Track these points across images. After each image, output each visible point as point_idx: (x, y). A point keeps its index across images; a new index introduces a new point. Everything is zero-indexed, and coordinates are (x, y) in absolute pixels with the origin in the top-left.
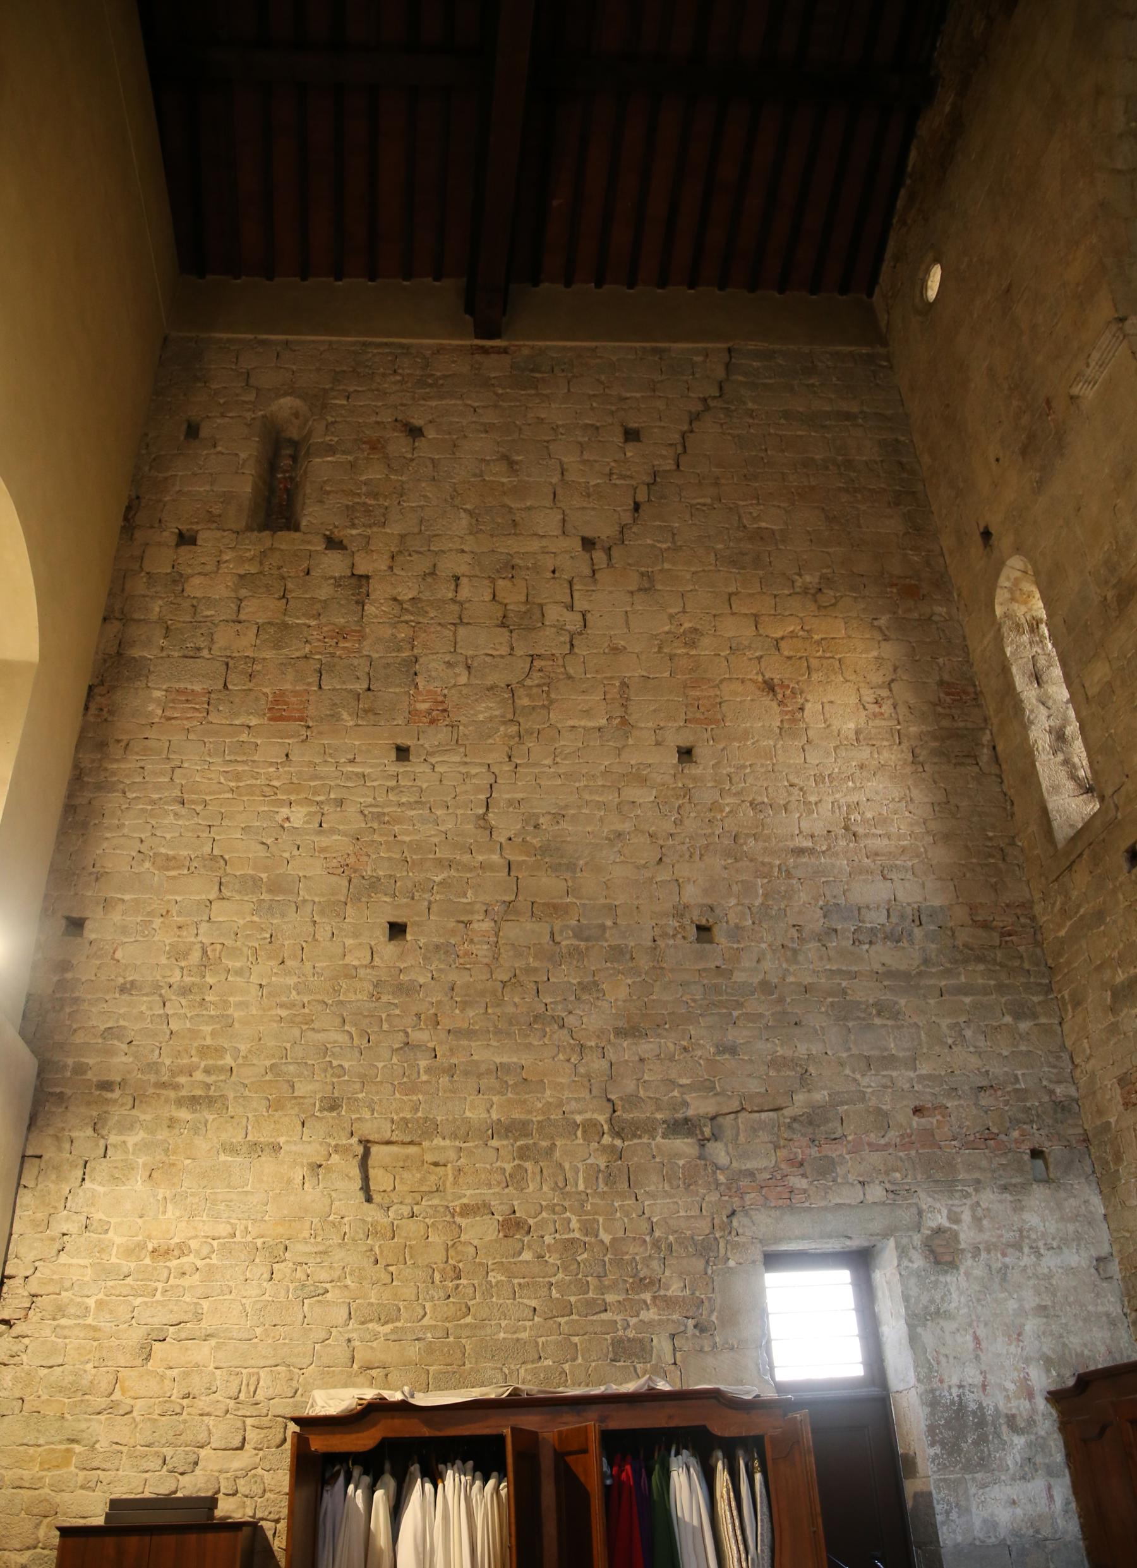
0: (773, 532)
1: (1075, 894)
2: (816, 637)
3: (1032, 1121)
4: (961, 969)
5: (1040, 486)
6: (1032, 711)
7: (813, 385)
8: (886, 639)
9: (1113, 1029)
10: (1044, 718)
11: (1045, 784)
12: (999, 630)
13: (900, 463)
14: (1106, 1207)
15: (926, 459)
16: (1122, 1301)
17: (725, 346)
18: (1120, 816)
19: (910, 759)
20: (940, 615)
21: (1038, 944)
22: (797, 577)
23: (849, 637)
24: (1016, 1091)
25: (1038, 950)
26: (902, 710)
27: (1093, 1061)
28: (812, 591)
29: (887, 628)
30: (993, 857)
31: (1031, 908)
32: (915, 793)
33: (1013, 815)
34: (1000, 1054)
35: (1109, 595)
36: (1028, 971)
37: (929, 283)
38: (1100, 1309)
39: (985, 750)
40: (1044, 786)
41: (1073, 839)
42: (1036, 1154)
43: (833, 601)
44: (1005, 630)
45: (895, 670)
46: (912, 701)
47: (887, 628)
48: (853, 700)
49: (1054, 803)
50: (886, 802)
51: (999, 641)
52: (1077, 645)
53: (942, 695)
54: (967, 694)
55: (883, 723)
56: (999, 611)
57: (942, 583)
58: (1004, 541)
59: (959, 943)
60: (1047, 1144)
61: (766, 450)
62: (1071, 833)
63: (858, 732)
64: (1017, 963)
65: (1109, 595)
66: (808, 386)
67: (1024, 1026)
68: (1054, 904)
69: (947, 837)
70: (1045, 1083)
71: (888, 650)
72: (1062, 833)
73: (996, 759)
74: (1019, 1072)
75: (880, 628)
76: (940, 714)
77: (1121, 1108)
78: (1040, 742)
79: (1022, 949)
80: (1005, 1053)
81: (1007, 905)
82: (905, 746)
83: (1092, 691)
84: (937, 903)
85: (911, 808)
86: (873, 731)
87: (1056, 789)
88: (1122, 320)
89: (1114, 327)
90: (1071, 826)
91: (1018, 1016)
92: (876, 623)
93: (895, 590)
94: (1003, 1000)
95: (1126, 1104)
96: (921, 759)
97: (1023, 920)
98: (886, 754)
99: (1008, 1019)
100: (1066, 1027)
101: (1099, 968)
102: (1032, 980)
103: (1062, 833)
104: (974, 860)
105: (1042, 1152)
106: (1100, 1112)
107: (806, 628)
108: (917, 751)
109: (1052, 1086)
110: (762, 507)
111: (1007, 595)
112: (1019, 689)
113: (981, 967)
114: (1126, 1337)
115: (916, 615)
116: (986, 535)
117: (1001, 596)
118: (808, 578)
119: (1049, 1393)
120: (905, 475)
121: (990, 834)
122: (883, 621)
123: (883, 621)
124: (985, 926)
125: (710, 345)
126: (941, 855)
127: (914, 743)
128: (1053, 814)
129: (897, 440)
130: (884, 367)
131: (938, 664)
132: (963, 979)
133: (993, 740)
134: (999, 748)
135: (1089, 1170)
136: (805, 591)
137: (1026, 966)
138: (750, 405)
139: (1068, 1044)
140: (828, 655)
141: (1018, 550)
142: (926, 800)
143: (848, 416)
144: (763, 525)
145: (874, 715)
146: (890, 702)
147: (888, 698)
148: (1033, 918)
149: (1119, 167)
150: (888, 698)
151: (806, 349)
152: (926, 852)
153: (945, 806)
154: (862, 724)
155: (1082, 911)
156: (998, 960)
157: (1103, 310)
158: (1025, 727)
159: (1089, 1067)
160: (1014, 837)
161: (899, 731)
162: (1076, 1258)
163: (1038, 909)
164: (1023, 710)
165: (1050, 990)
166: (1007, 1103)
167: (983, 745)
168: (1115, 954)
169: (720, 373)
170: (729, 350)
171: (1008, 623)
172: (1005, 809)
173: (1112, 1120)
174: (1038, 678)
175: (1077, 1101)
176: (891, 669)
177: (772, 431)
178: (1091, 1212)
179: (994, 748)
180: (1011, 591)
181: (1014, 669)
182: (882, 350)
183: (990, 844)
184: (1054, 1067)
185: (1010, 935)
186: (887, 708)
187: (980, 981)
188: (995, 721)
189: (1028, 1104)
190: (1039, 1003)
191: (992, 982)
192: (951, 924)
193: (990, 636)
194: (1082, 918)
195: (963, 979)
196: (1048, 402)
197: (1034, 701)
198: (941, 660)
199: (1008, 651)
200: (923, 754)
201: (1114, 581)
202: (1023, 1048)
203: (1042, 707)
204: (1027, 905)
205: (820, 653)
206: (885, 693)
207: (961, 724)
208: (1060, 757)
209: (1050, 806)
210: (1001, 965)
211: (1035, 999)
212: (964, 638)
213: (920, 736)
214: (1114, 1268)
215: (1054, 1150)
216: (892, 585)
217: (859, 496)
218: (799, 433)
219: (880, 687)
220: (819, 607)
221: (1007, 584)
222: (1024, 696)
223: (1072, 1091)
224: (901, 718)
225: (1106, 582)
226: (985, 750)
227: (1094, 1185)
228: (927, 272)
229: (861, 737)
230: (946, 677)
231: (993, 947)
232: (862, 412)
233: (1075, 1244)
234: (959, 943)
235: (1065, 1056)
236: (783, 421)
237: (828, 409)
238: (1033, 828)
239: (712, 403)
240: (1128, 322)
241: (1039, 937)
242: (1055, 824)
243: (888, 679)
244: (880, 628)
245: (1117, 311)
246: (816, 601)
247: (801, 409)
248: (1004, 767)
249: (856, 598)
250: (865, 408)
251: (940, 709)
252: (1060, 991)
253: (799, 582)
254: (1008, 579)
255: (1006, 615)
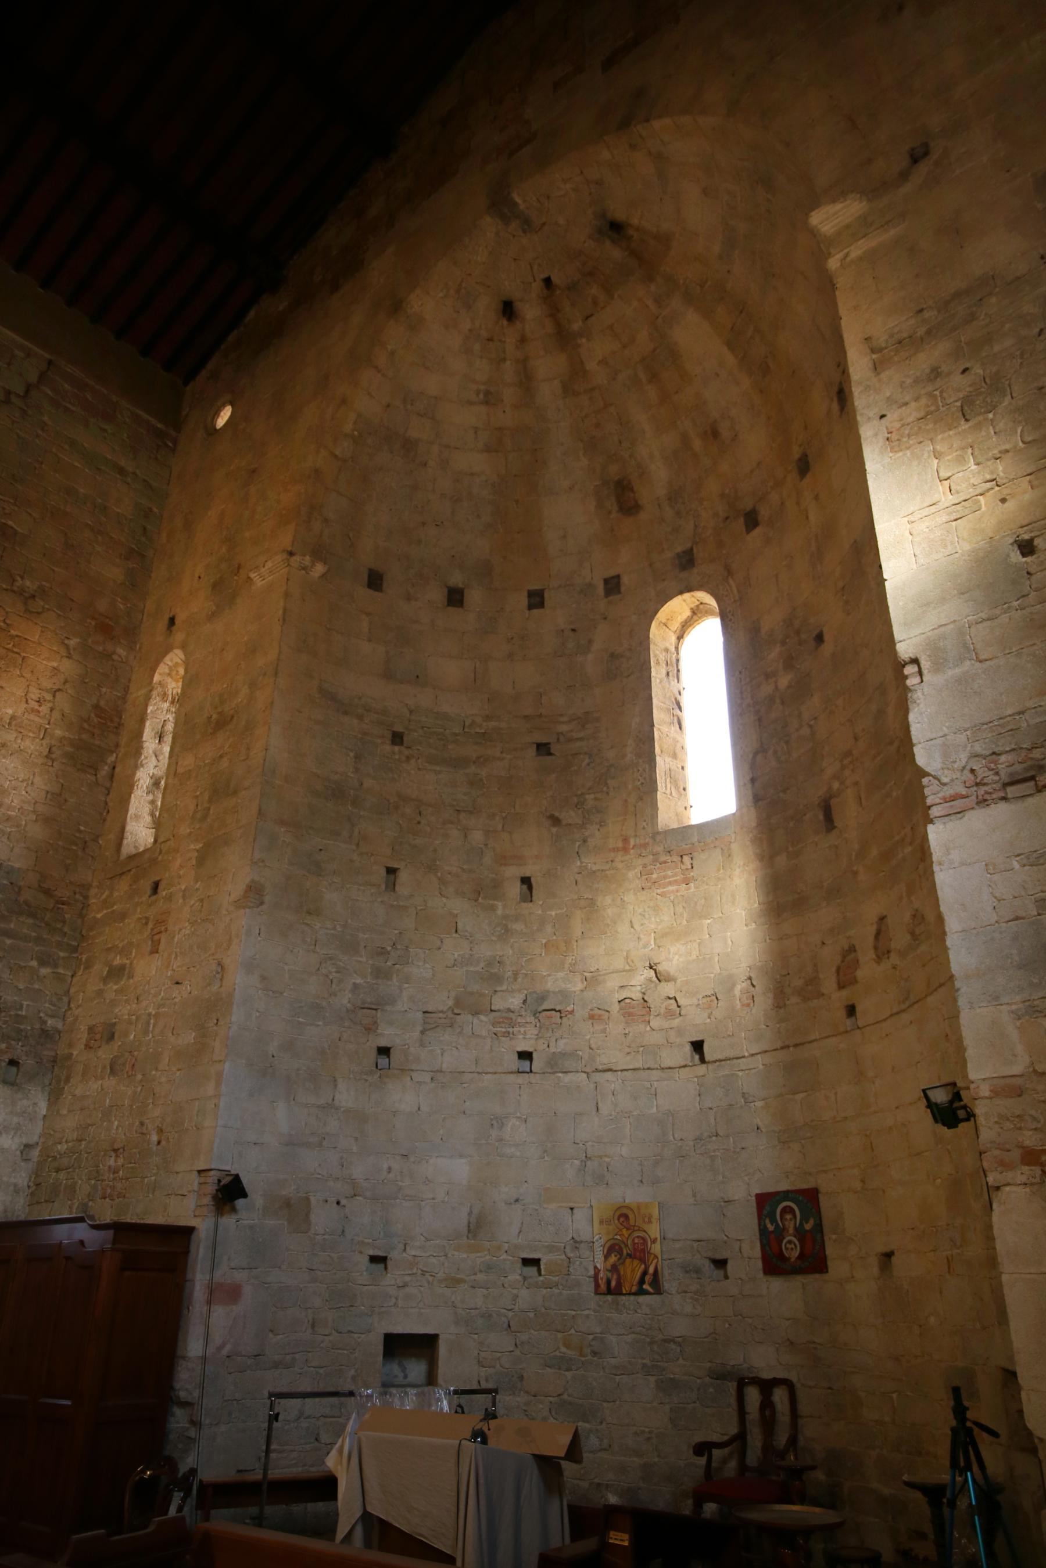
0: (16, 532)
1: (116, 894)
2: (13, 632)
3: (19, 1040)
4: (14, 919)
5: (212, 617)
6: (146, 758)
7: (105, 430)
8: (69, 657)
9: (100, 993)
10: (152, 766)
11: (132, 811)
12: (151, 691)
13: (145, 529)
14: (48, 1110)
15: (164, 535)
16: (30, 1177)
17: (47, 356)
18: (160, 858)
19: (45, 753)
20: (120, 656)
21: (81, 916)
22: (19, 578)
23: (40, 644)
24: (18, 1015)
25: (79, 921)
26: (56, 715)
27: (80, 1010)
28: (27, 595)
29: (74, 649)
30: (77, 845)
31: (88, 889)
32: (38, 780)
33: (104, 820)
34: (16, 987)
35: (215, 716)
36: (65, 933)
37: (222, 414)
38: (13, 1180)
39: (106, 768)
40: (130, 813)
41: (131, 858)
42: (13, 1063)
43: (40, 610)
44: (154, 693)
45: (64, 683)
46: (67, 711)
47: (74, 649)
48: (20, 693)
49: (131, 826)
50: (10, 778)
51: (148, 698)
52: (187, 735)
53: (93, 715)
54: (112, 721)
55: (37, 719)
56: (157, 678)
57: (131, 633)
58: (179, 636)
59: (21, 899)
60: (24, 1058)
61: (42, 463)
62: (134, 851)
63: (13, 718)
64: (59, 926)
65: (215, 716)
66: (101, 429)
67: (44, 971)
68: (102, 894)
69: (48, 821)
70: (42, 1015)
71: (68, 667)
72: (127, 849)
73: (112, 777)
74: (25, 1003)
75: (67, 647)
76: (84, 729)
77: (83, 1047)
78: (141, 781)
79: (67, 916)
80: (21, 986)
81: (71, 883)
82: (44, 742)
83: (180, 770)
84: (17, 865)
85: (29, 789)
86: (25, 722)
87: (137, 817)
88: (291, 554)
89: (285, 556)
90: (136, 847)
91: (43, 963)
92: (66, 641)
93: (93, 623)
94: (37, 949)
95: (86, 1046)
96: (53, 756)
97: (78, 896)
98: (28, 743)
99: (34, 963)
100: (75, 979)
101: (109, 950)
102: (65, 940)
103: (127, 849)
104: (60, 843)
105: (18, 1063)
106: (71, 1045)
107: (8, 622)
108: (54, 749)
109: (46, 1018)
110: (16, 508)
111: (167, 671)
112: (144, 739)
113: (30, 921)
114: (22, 1201)
115: (101, 649)
116: (172, 621)
117: (162, 668)
118: (28, 583)
119: (156, 1256)
120: (143, 539)
121: (82, 828)
122: (73, 642)
123: (73, 642)
124: (47, 892)
125: (36, 349)
126: (37, 832)
127: (53, 742)
128: (127, 834)
129: (151, 510)
130: (167, 446)
131: (100, 691)
132: (12, 926)
133: (115, 762)
134: (117, 770)
135: (47, 1082)
136: (21, 592)
137: (66, 929)
138: (45, 418)
139: (72, 991)
140: (15, 650)
141: (183, 647)
142: (43, 787)
143: (121, 471)
144: (10, 523)
145: (33, 710)
146: (50, 705)
147: (50, 701)
148: (86, 897)
149: (337, 453)
150: (50, 701)
151: (114, 398)
152: (26, 825)
153: (57, 798)
154: (19, 713)
155: (115, 907)
156: (46, 919)
157: (286, 539)
158: (136, 767)
159: (77, 1012)
160: (98, 836)
161: (46, 729)
162: (10, 1142)
163: (93, 891)
164: (140, 754)
165: (75, 949)
166: (6, 1022)
167: (106, 764)
168: (120, 945)
169: (33, 377)
170: (50, 362)
171: (160, 689)
172: (101, 814)
173: (75, 1053)
174: (161, 737)
175: (60, 1032)
176: (62, 681)
177: (54, 450)
178: (35, 1112)
179: (114, 768)
180: (170, 669)
181: (148, 724)
182: (173, 433)
183: (78, 835)
184: (54, 1005)
185: (63, 904)
186: (44, 709)
187: (25, 931)
188: (122, 750)
189: (22, 1027)
190: (63, 958)
191: (34, 934)
192: (22, 883)
193: (143, 691)
194: (113, 912)
195: (12, 926)
196: (239, 567)
197: (151, 752)
198: (104, 690)
199: (150, 709)
200: (57, 753)
201: (220, 710)
202: (36, 986)
203: (154, 758)
204: (86, 887)
205: (10, 646)
206: (49, 697)
207: (97, 742)
208: (150, 797)
209: (128, 828)
210: (47, 924)
211: (62, 954)
212: (130, 680)
213: (61, 739)
214: (35, 1154)
215: (28, 1063)
216: (93, 618)
217: (100, 538)
218: (76, 464)
219: (47, 691)
220: (26, 610)
221: (170, 663)
222: (145, 745)
223: (60, 1026)
224: (52, 720)
225: (216, 708)
226: (106, 768)
227: (46, 1094)
228: (224, 406)
229: (14, 723)
230: (102, 703)
231: (47, 909)
232: (134, 473)
233: (12, 1133)
234: (21, 899)
235: (65, 999)
236: (66, 447)
237: (109, 457)
238: (112, 836)
239: (14, 399)
240: (295, 558)
241: (84, 912)
242: (125, 842)
243: (56, 687)
244: (67, 647)
245: (293, 545)
246: (25, 604)
247: (86, 445)
248: (114, 785)
249: (59, 615)
250: (138, 471)
251: (86, 725)
252: (81, 954)
253: (19, 582)
254: (171, 660)
255: (160, 683)
